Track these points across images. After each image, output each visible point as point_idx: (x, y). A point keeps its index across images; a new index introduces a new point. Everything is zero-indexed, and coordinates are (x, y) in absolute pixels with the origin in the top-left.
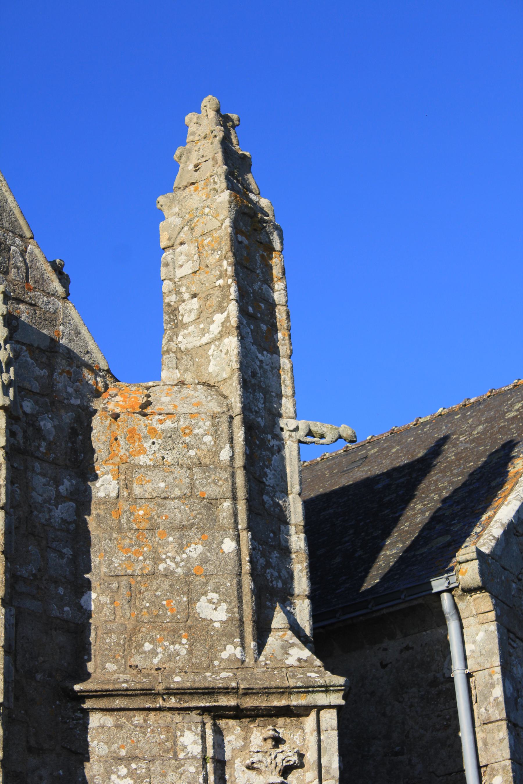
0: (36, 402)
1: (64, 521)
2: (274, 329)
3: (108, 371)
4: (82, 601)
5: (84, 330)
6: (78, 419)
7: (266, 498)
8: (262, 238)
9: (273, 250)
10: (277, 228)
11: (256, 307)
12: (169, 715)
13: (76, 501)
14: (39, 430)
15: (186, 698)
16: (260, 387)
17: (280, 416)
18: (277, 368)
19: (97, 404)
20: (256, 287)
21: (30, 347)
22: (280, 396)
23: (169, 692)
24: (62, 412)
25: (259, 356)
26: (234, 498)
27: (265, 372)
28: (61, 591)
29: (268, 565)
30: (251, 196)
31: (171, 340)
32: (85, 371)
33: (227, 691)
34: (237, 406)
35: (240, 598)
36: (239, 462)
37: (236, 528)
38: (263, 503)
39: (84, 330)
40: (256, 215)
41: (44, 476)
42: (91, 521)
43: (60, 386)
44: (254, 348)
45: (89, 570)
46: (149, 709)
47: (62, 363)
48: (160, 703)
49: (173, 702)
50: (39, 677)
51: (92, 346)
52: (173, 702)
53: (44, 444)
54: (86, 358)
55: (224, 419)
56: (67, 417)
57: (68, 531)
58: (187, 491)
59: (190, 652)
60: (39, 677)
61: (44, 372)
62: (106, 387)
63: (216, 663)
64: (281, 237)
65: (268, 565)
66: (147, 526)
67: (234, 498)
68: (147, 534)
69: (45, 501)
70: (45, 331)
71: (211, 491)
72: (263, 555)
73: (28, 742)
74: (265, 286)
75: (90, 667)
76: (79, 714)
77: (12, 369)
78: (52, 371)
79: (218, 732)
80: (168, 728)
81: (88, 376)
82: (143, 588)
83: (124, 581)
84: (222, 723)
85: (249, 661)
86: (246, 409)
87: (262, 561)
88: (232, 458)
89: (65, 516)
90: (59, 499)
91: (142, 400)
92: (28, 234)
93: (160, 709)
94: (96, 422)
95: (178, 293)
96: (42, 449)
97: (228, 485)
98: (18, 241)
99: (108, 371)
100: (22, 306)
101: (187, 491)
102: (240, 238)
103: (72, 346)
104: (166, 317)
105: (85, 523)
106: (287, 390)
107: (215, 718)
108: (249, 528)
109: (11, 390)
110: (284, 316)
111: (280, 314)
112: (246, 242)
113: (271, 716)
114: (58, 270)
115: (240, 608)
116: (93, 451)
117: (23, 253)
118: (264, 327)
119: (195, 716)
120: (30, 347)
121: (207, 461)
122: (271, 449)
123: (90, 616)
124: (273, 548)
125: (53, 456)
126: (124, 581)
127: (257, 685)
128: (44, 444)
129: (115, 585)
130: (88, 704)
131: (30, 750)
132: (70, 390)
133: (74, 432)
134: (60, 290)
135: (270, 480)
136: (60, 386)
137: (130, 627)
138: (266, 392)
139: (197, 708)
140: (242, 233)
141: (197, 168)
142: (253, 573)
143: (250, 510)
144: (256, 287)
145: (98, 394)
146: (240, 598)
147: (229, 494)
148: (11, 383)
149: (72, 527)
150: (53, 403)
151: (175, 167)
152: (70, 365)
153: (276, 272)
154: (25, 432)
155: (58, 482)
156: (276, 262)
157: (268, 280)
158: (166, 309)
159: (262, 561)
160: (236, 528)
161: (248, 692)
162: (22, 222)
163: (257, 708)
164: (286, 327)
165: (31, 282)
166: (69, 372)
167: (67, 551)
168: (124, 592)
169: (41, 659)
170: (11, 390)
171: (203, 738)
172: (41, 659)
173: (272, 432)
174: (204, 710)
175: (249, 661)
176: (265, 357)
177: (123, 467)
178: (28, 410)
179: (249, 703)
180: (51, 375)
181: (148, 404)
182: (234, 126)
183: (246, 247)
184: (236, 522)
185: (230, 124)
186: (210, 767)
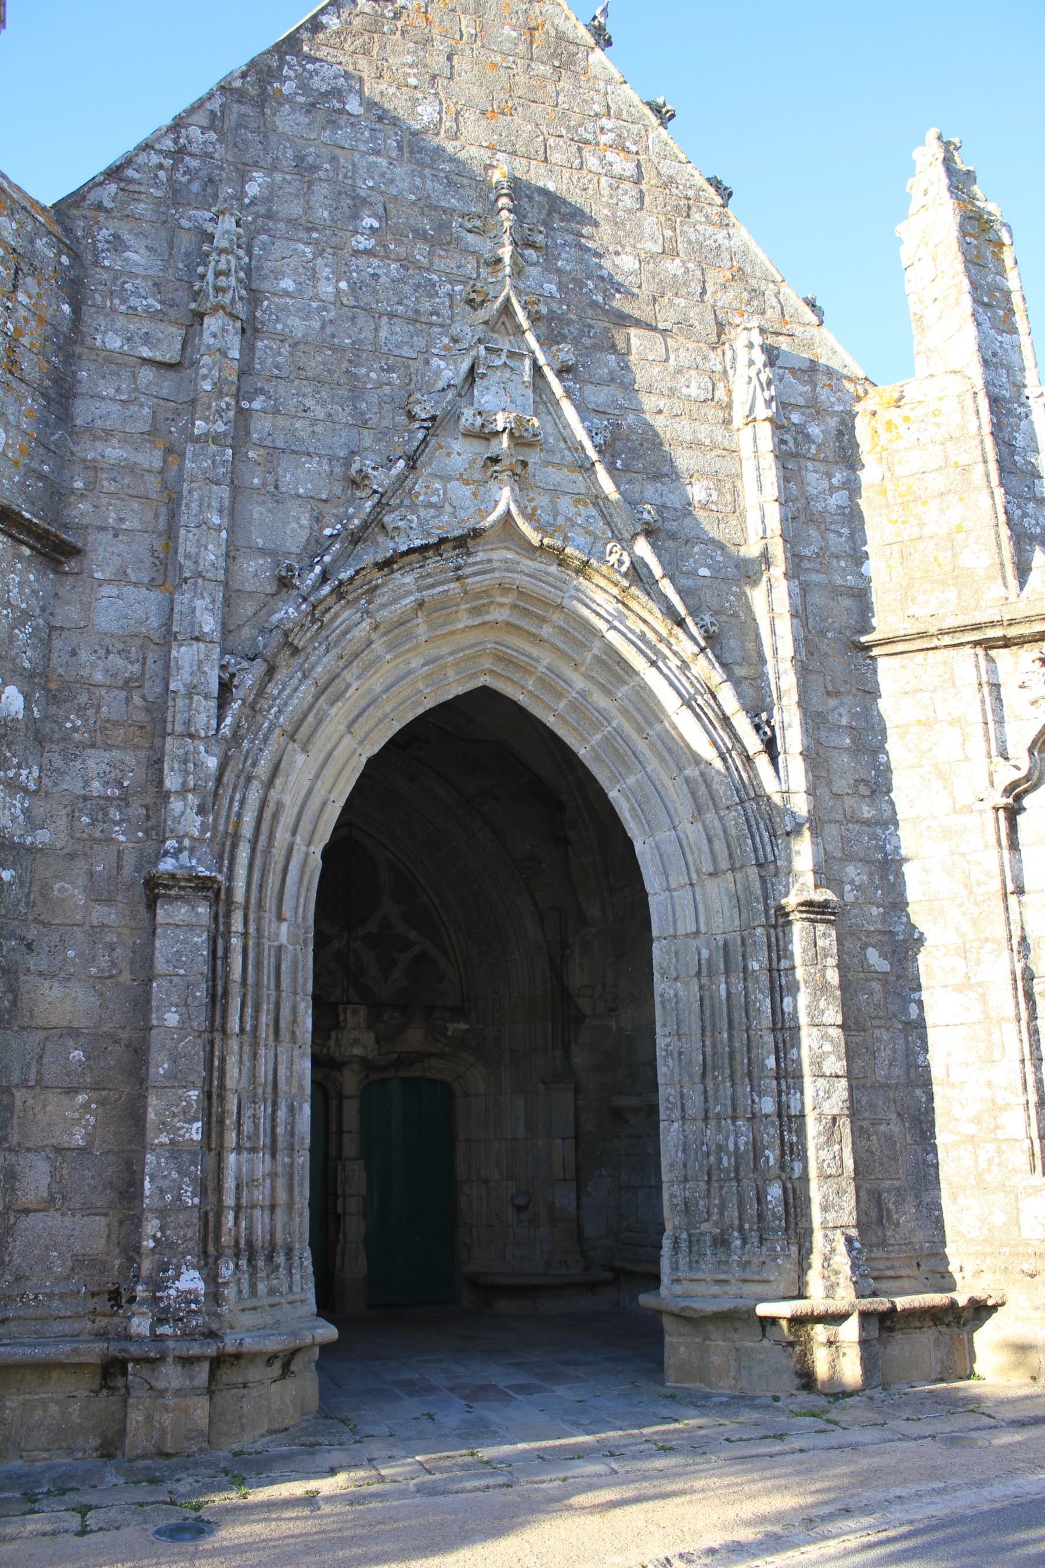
0: (803, 414)
1: (839, 507)
2: (1011, 312)
3: (866, 379)
4: (863, 570)
5: (838, 348)
6: (843, 422)
7: (1016, 458)
8: (992, 236)
9: (1003, 245)
10: (1004, 225)
11: (992, 296)
12: (945, 651)
13: (848, 489)
14: (807, 436)
15: (957, 635)
16: (1002, 364)
17: (1025, 386)
18: (1017, 347)
19: (858, 407)
20: (989, 279)
21: (792, 370)
22: (1023, 369)
23: (942, 633)
24: (828, 418)
25: (999, 338)
26: (985, 462)
27: (1006, 351)
28: (843, 564)
29: (1025, 515)
30: (978, 203)
31: (920, 343)
32: (845, 382)
33: (992, 624)
34: (979, 384)
35: (999, 546)
36: (987, 428)
37: (989, 486)
38: (1015, 463)
39: (838, 348)
40: (981, 216)
41: (817, 472)
42: (863, 503)
43: (823, 397)
44: (992, 332)
45: (865, 543)
46: (927, 649)
47: (822, 379)
48: (935, 642)
49: (947, 640)
50: (829, 635)
51: (849, 361)
52: (947, 640)
53: (813, 447)
54: (845, 371)
55: (970, 395)
56: (833, 422)
57: (844, 514)
58: (943, 463)
59: (959, 597)
60: (829, 635)
61: (808, 388)
62: (866, 392)
63: (982, 603)
64: (1010, 231)
65: (1025, 515)
66: (911, 498)
67: (985, 462)
68: (911, 505)
69: (820, 493)
70: (805, 355)
71: (963, 459)
72: (1019, 507)
73: (108, 434)
74: (998, 278)
75: (874, 622)
76: (868, 661)
77: (772, 388)
78: (814, 386)
79: (991, 660)
80: (945, 663)
81: (848, 386)
82: (912, 550)
83: (896, 548)
84: (993, 653)
85: (1013, 598)
86: (987, 384)
87: (1019, 512)
88: (980, 427)
89: (839, 503)
90: (832, 489)
91: (896, 396)
92: (779, 279)
93: (936, 648)
94: (858, 422)
95: (921, 302)
96: (813, 451)
97: (979, 452)
98: (771, 285)
99: (866, 379)
100: (781, 338)
101: (943, 463)
102: (968, 239)
103: (830, 364)
104: (913, 325)
105: (858, 505)
106: (1028, 363)
107: (986, 649)
108: (1001, 485)
109: (774, 404)
110: (1020, 299)
111: (1016, 299)
112: (975, 242)
113: (1037, 641)
114: (812, 304)
115: (1000, 553)
116: (858, 445)
117: (777, 295)
118: (1001, 313)
119: (968, 650)
120: (792, 370)
121: (957, 435)
122: (1019, 416)
123: (870, 581)
124: (1029, 499)
125: (822, 455)
126: (896, 548)
127: (1018, 615)
128: (813, 447)
129: (888, 553)
130: (875, 652)
131: (828, 693)
132: (833, 399)
133: (840, 433)
134: (814, 320)
135: (1020, 442)
136: (823, 397)
137: (904, 584)
138: (1009, 368)
139: (969, 643)
140: (971, 235)
141: (926, 192)
142: (1009, 522)
143: (1001, 469)
144: (989, 279)
145: (858, 399)
146: (999, 546)
147: (980, 459)
148: (772, 398)
149: (847, 511)
150: (818, 412)
151: (908, 198)
152: (830, 379)
153: (1009, 263)
154: (795, 439)
155: (829, 476)
156: (1007, 256)
157: (1001, 272)
158: (912, 318)
159: (1019, 512)
160: (989, 486)
161: (1012, 623)
162: (772, 270)
163: (1022, 636)
164: (591, 41)
165: (787, 317)
166: (830, 385)
167: (845, 531)
168: (897, 556)
169: (830, 620)
170: (774, 404)
171: (977, 667)
172: (830, 620)
173: (1018, 401)
174: (976, 643)
175: (1013, 598)
176: (1006, 338)
177: (884, 454)
178: (796, 421)
179: (1013, 632)
180: (814, 390)
181: (901, 398)
182: (957, 149)
183: (976, 247)
184: (988, 481)
185: (952, 147)
186: (986, 689)
